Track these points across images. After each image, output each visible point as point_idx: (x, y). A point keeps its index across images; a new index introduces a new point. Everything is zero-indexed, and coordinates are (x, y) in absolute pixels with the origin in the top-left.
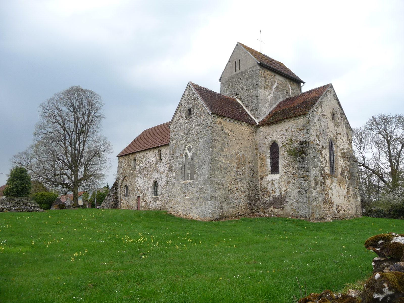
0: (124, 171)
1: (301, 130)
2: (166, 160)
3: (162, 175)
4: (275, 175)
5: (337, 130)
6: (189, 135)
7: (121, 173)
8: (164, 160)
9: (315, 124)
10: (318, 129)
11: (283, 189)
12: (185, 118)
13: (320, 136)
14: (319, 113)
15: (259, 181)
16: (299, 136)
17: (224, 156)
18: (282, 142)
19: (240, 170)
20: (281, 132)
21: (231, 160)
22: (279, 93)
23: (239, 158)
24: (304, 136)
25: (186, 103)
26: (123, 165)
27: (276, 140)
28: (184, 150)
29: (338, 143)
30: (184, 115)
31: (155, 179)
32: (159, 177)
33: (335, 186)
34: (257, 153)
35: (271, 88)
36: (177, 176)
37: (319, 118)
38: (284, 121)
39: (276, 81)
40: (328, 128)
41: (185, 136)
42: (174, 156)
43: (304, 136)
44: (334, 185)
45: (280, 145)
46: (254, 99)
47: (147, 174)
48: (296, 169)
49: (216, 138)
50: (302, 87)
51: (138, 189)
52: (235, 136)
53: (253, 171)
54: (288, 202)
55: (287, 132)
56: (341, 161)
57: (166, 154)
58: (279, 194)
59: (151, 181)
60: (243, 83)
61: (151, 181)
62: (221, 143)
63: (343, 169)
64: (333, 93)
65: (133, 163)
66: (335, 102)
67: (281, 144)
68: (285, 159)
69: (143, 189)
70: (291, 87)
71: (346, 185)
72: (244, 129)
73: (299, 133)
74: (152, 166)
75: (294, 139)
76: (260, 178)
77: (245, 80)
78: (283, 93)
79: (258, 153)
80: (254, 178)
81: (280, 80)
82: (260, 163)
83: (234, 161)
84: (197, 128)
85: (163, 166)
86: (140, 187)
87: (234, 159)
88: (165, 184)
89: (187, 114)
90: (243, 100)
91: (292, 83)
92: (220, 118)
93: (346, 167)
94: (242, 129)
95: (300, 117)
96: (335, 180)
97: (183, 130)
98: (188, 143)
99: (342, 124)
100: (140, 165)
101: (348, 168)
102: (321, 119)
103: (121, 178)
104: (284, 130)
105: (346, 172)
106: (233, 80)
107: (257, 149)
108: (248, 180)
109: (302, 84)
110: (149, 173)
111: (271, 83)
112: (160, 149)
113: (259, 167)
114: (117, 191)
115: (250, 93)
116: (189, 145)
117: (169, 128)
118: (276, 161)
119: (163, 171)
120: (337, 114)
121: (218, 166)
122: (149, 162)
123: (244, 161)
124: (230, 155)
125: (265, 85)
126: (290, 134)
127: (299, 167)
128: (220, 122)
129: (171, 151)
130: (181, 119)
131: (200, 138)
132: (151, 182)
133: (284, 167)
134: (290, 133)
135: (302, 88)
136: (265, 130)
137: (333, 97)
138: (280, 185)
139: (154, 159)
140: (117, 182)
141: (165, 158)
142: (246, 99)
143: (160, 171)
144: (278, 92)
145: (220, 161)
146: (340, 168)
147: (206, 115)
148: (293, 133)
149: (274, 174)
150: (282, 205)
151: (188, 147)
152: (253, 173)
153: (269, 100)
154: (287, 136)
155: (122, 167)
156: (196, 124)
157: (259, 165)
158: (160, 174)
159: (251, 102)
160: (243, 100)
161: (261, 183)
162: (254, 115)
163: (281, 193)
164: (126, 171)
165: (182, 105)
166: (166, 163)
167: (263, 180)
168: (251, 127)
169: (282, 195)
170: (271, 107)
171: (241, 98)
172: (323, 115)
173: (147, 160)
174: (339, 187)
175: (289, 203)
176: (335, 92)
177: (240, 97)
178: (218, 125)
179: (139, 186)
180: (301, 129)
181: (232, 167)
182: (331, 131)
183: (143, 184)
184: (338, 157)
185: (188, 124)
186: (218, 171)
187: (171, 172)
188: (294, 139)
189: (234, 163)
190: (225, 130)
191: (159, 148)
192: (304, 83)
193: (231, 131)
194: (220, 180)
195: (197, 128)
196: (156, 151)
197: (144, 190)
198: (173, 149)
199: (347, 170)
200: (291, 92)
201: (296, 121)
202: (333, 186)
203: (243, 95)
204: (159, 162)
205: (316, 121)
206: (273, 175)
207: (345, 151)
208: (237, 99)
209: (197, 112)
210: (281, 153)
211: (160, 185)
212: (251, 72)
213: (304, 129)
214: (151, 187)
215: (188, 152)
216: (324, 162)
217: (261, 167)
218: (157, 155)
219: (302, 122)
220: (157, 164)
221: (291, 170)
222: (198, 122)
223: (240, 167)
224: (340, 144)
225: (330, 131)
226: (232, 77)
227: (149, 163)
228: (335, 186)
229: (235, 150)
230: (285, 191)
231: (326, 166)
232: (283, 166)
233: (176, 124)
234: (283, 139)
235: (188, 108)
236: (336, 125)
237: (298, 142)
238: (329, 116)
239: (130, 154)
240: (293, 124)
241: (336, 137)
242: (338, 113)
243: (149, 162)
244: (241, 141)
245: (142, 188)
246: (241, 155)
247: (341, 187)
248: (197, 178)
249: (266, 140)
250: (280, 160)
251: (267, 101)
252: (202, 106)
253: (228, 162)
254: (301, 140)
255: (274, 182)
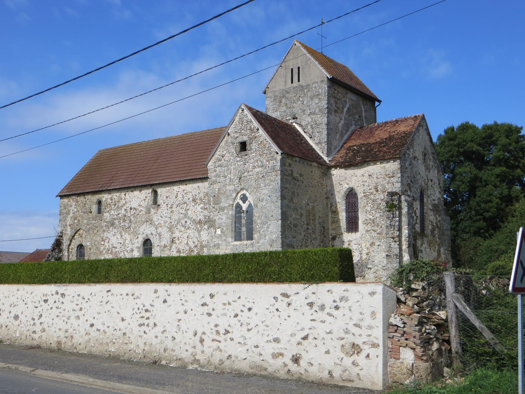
0: (76, 221)
1: (389, 177)
2: (169, 206)
3: (160, 230)
4: (354, 234)
5: (428, 175)
6: (243, 178)
7: (68, 224)
8: (163, 207)
9: (406, 170)
10: (409, 176)
11: (365, 252)
12: (235, 155)
13: (411, 185)
14: (411, 156)
15: (329, 241)
16: (386, 184)
17: (294, 209)
18: (364, 190)
19: (310, 228)
20: (362, 178)
21: (301, 214)
22: (350, 118)
23: (308, 211)
24: (393, 185)
25: (236, 132)
26: (73, 210)
27: (355, 188)
28: (235, 199)
29: (429, 193)
30: (233, 150)
31: (147, 235)
32: (154, 233)
33: (425, 248)
34: (327, 204)
35: (342, 112)
36: (223, 234)
37: (411, 161)
38: (368, 164)
39: (348, 101)
40: (419, 174)
41: (235, 180)
42: (216, 206)
43: (393, 185)
44: (424, 247)
45: (360, 195)
46: (322, 129)
47: (129, 227)
48: (383, 226)
49: (285, 186)
50: (377, 107)
51: (109, 250)
52: (304, 181)
53: (324, 228)
54: (371, 269)
55: (371, 178)
56: (431, 215)
57: (167, 197)
58: (359, 259)
59: (137, 238)
60: (305, 103)
61: (137, 238)
62: (290, 192)
63: (433, 225)
64: (425, 127)
65: (95, 208)
66: (427, 137)
67: (362, 193)
68: (368, 213)
69: (121, 252)
70: (364, 107)
71: (436, 246)
72: (313, 171)
73: (387, 181)
74: (138, 214)
75: (379, 188)
76: (331, 237)
77: (309, 99)
78: (355, 118)
79: (329, 203)
80: (325, 237)
81: (351, 99)
82: (332, 217)
83: (304, 215)
84: (257, 170)
85: (162, 215)
86: (113, 249)
87: (304, 212)
88: (166, 244)
89: (238, 149)
90: (305, 126)
91: (365, 103)
92: (290, 158)
93: (436, 223)
94: (312, 172)
95: (388, 161)
96: (425, 239)
97: (232, 171)
98: (242, 189)
99: (434, 167)
100: (112, 212)
101: (439, 225)
102: (412, 163)
103: (69, 232)
104: (367, 175)
105: (437, 230)
106: (287, 95)
107: (327, 198)
108: (318, 240)
109: (377, 103)
110: (133, 225)
111: (342, 104)
112: (155, 187)
113: (330, 222)
114: (61, 255)
115: (316, 119)
116: (244, 192)
117: (207, 165)
118: (355, 215)
119: (162, 223)
120: (428, 154)
121: (289, 222)
122: (133, 208)
123: (314, 215)
124: (300, 208)
125: (336, 108)
126: (374, 181)
127: (388, 225)
128: (289, 164)
129: (212, 199)
130: (229, 155)
131: (262, 185)
132: (137, 240)
133: (365, 224)
134: (375, 180)
135: (377, 108)
136: (339, 173)
137: (425, 133)
138: (359, 246)
139: (144, 204)
140: (60, 239)
141: (166, 203)
142: (309, 127)
143: (157, 224)
144: (349, 116)
145: (291, 217)
146: (430, 224)
147: (272, 155)
148: (379, 180)
149: (352, 232)
150: (362, 272)
151: (241, 195)
152: (324, 231)
153: (340, 129)
154: (372, 183)
155: (71, 215)
156: (256, 164)
157: (330, 220)
158: (156, 229)
159: (318, 132)
160: (305, 126)
161: (333, 244)
162: (323, 150)
163: (361, 257)
164: (79, 220)
165: (229, 135)
166: (169, 211)
167: (335, 240)
168: (322, 168)
169: (363, 259)
170: (342, 139)
171: (301, 124)
172: (415, 157)
173: (127, 205)
174: (429, 249)
175: (372, 270)
176: (427, 126)
177: (299, 122)
178: (287, 168)
179: (111, 246)
180: (389, 176)
181: (302, 224)
182: (423, 178)
183: (121, 243)
184: (429, 211)
185: (241, 163)
186: (288, 229)
187: (212, 228)
188: (381, 188)
189: (304, 218)
190: (295, 175)
191: (153, 187)
192: (380, 101)
193: (301, 175)
194: (291, 241)
195: (257, 170)
196: (147, 193)
197: (124, 253)
198: (215, 196)
199: (437, 226)
200: (363, 115)
201: (383, 165)
202: (423, 249)
203: (305, 120)
204: (154, 208)
205: (407, 166)
206: (350, 234)
207: (436, 202)
208: (294, 124)
209: (257, 149)
210: (362, 205)
211: (158, 246)
212: (318, 88)
213: (394, 176)
214: (138, 248)
215: (241, 202)
216: (415, 217)
217: (333, 222)
218: (149, 198)
219: (392, 168)
220: (148, 211)
221: (376, 228)
222: (259, 162)
223: (310, 223)
224: (431, 194)
225: (421, 177)
226: (285, 90)
227: (131, 209)
228: (425, 248)
229: (305, 201)
230: (367, 254)
231: (416, 223)
232: (364, 222)
233: (220, 160)
234: (365, 187)
235: (240, 140)
236: (428, 169)
237: (385, 192)
238: (421, 157)
239: (88, 193)
240: (379, 168)
241: (427, 184)
242: (429, 152)
243: (133, 208)
244: (311, 188)
245: (117, 250)
246: (311, 207)
247: (432, 249)
248: (260, 238)
249: (341, 186)
250: (359, 215)
251: (337, 131)
252: (265, 141)
253: (299, 217)
254: (390, 191)
255: (351, 243)
